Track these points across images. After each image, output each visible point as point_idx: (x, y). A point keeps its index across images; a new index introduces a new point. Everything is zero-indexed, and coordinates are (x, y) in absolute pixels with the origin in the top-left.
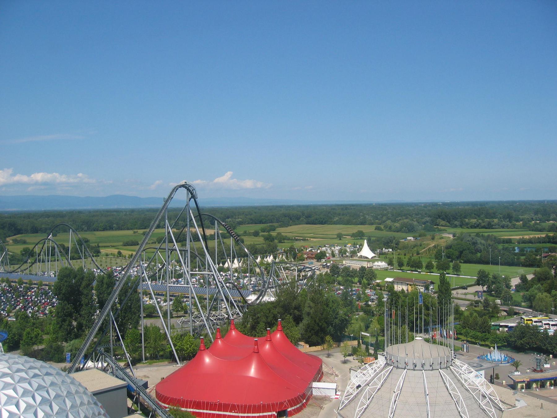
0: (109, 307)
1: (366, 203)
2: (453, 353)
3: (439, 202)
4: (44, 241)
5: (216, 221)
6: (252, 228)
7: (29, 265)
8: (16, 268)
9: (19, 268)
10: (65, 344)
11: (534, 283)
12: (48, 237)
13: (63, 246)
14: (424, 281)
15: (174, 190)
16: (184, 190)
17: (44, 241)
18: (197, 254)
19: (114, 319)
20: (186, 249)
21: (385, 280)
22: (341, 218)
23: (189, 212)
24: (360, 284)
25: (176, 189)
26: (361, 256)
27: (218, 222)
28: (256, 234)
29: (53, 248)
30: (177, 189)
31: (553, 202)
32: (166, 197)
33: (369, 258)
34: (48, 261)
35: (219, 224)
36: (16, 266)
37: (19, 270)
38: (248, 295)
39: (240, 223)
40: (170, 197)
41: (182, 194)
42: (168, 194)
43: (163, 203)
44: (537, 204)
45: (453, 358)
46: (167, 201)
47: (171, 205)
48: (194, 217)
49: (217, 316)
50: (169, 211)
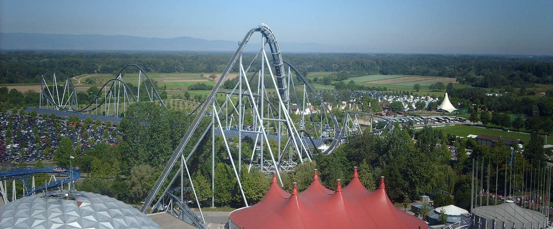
0: (181, 150)
1: (349, 52)
2: (548, 220)
3: (528, 56)
4: (112, 82)
5: (289, 68)
6: (322, 75)
7: (97, 105)
8: (84, 108)
9: (88, 107)
10: (365, 163)
11: (156, 199)
12: (117, 78)
13: (131, 86)
14: (511, 139)
15: (249, 33)
16: (259, 34)
17: (112, 82)
18: (268, 101)
19: (185, 163)
20: (256, 95)
21: (468, 137)
22: (417, 69)
23: (240, 56)
24: (90, 168)
25: (250, 33)
26: (441, 109)
27: (291, 68)
28: (326, 82)
29: (122, 89)
30: (253, 32)
31: (551, 58)
32: (241, 41)
33: (449, 113)
34: (108, 102)
35: (292, 69)
36: (84, 106)
37: (88, 109)
38: (320, 145)
39: (310, 70)
40: (245, 41)
41: (257, 38)
42: (243, 37)
43: (238, 47)
44: (325, 61)
45: (548, 225)
46: (241, 45)
47: (246, 49)
48: (269, 61)
49: (288, 165)
50: (244, 55)
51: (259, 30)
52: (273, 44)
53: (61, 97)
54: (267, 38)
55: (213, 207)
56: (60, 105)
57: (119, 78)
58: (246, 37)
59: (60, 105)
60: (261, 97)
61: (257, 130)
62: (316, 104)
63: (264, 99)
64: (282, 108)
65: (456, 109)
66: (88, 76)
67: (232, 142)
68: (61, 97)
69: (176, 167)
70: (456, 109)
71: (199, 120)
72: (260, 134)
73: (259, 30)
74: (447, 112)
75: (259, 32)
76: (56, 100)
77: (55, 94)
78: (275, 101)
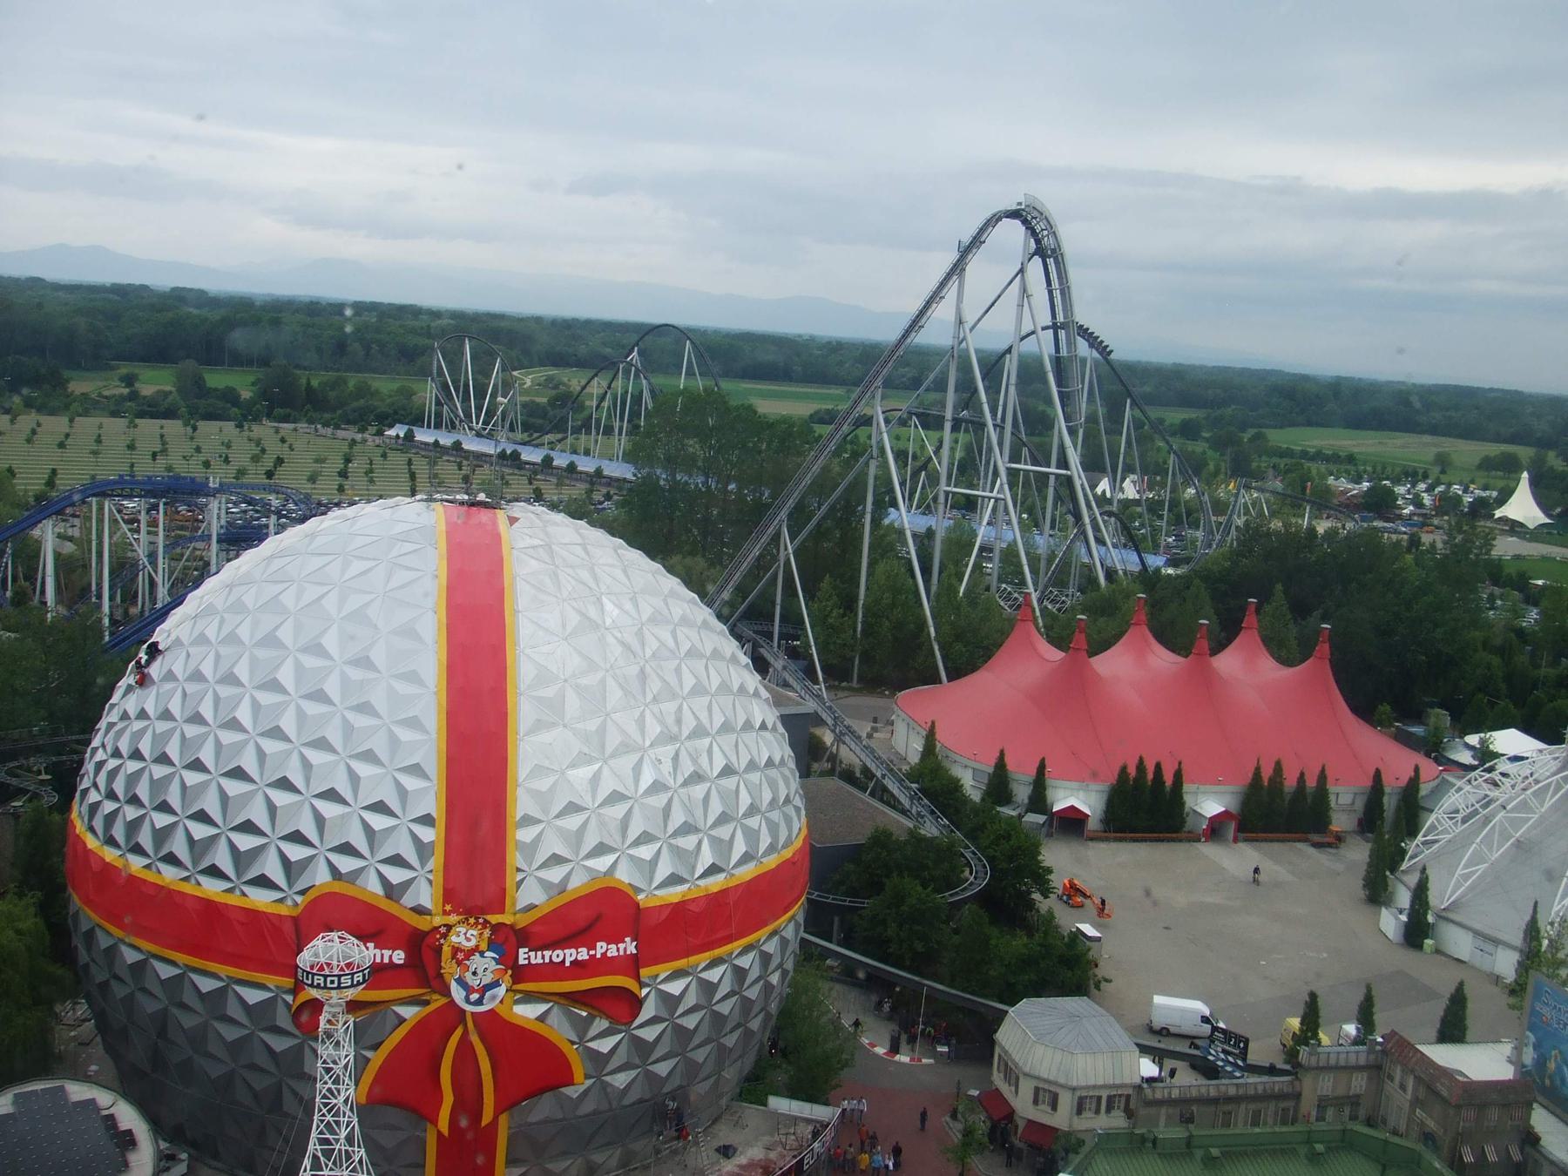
19: (790, 551)
30: (999, 219)
32: (967, 240)
42: (973, 231)
43: (954, 256)
51: (1014, 214)
52: (1052, 259)
53: (479, 409)
54: (1038, 242)
55: (855, 684)
56: (477, 423)
57: (632, 359)
58: (982, 230)
59: (477, 423)
60: (1003, 428)
61: (992, 491)
62: (1152, 471)
63: (1012, 433)
64: (1060, 432)
65: (1548, 521)
66: (553, 372)
67: (964, 339)
68: (479, 409)
69: (763, 564)
70: (1548, 521)
71: (835, 441)
72: (997, 500)
73: (1014, 214)
74: (1521, 525)
75: (1017, 223)
76: (468, 415)
77: (466, 399)
78: (1046, 424)
